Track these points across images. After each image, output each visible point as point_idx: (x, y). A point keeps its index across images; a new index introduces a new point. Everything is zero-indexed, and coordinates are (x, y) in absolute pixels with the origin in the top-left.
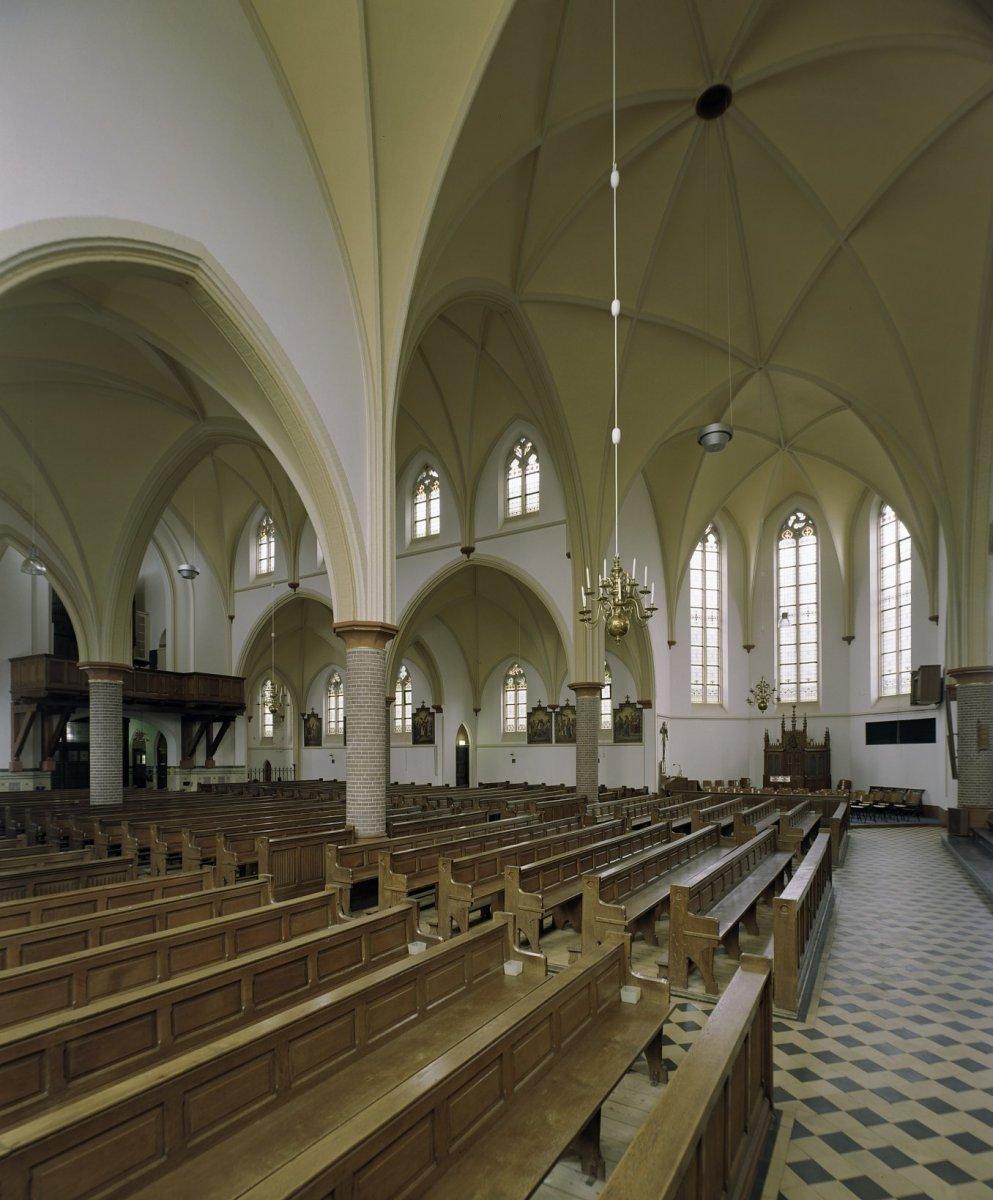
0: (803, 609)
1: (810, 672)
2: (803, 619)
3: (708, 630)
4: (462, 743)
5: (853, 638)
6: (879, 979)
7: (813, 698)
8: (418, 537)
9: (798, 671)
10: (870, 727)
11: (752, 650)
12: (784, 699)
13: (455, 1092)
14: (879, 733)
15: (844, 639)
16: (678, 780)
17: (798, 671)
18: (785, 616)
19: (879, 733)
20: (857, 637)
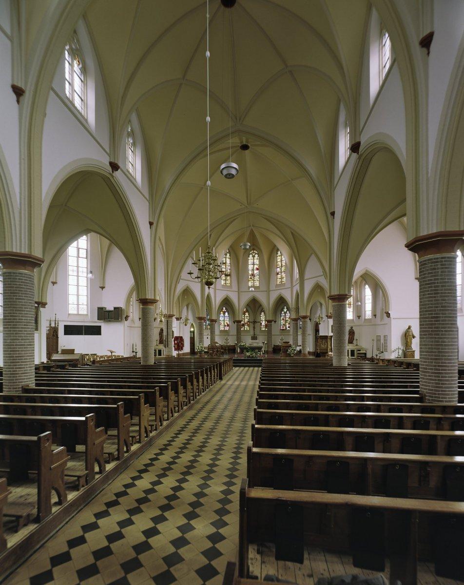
0: (80, 269)
1: (84, 300)
2: (80, 274)
3: (79, 277)
4: (192, 329)
5: (104, 287)
6: (356, 282)
7: (85, 313)
8: (85, 237)
9: (78, 299)
10: (66, 327)
11: (55, 285)
12: (71, 312)
13: (416, 177)
14: (71, 330)
15: (100, 287)
16: (389, 314)
17: (78, 299)
18: (301, 328)
19: (71, 330)
20: (106, 288)
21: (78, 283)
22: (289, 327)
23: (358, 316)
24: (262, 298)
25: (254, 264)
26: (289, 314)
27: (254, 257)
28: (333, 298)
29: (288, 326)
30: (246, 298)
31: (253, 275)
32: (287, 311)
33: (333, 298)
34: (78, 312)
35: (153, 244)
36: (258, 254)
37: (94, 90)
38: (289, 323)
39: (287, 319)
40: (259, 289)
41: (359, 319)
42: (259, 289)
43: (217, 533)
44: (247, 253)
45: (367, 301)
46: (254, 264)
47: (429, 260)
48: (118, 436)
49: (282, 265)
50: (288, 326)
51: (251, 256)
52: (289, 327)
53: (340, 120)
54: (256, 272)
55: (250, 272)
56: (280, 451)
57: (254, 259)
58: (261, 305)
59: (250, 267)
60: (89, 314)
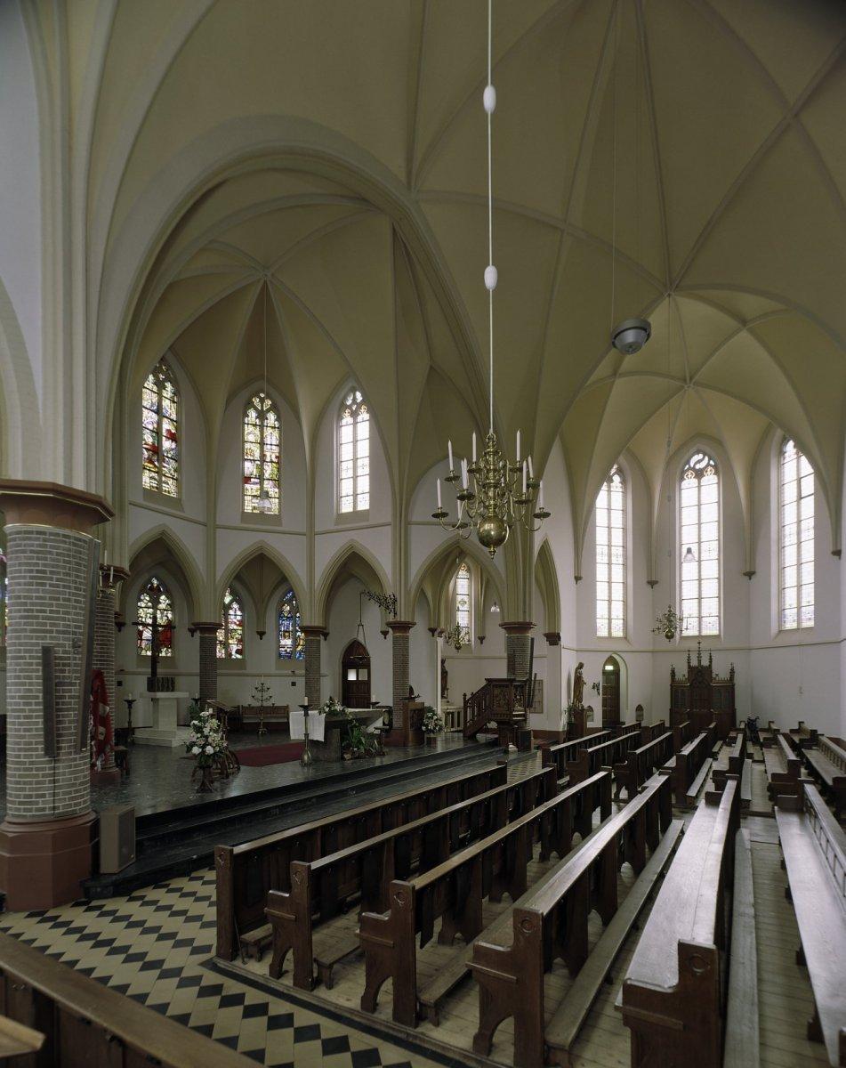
7: (715, 632)
9: (610, 608)
17: (610, 608)
21: (610, 596)
22: (237, 652)
23: (479, 638)
24: (290, 554)
25: (159, 411)
26: (239, 613)
27: (262, 415)
29: (234, 648)
31: (156, 450)
32: (231, 602)
34: (700, 631)
35: (575, 543)
36: (274, 408)
38: (240, 641)
39: (232, 626)
40: (281, 525)
41: (482, 643)
42: (281, 525)
44: (238, 403)
46: (159, 411)
50: (234, 648)
51: (252, 414)
52: (237, 652)
54: (167, 444)
55: (148, 438)
56: (457, 860)
57: (262, 427)
58: (283, 579)
59: (149, 418)
60: (722, 634)
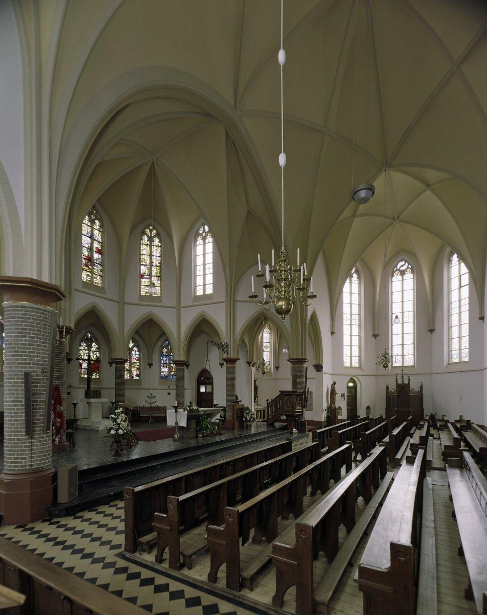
7: (412, 364)
9: (351, 350)
17: (351, 350)
22: (137, 375)
24: (167, 319)
25: (91, 237)
26: (137, 353)
28: (177, 363)
29: (135, 373)
30: (189, 318)
31: (90, 259)
32: (133, 347)
33: (177, 363)
34: (403, 363)
37: (418, 474)
38: (138, 369)
39: (134, 361)
40: (161, 302)
42: (161, 302)
43: (84, 554)
45: (220, 483)
46: (91, 237)
47: (22, 307)
48: (161, 372)
49: (151, 262)
50: (135, 373)
52: (137, 375)
53: (308, 311)
54: (96, 256)
55: (85, 252)
59: (86, 241)
60: (416, 365)
